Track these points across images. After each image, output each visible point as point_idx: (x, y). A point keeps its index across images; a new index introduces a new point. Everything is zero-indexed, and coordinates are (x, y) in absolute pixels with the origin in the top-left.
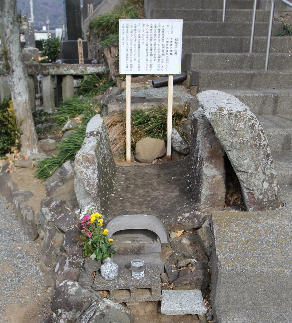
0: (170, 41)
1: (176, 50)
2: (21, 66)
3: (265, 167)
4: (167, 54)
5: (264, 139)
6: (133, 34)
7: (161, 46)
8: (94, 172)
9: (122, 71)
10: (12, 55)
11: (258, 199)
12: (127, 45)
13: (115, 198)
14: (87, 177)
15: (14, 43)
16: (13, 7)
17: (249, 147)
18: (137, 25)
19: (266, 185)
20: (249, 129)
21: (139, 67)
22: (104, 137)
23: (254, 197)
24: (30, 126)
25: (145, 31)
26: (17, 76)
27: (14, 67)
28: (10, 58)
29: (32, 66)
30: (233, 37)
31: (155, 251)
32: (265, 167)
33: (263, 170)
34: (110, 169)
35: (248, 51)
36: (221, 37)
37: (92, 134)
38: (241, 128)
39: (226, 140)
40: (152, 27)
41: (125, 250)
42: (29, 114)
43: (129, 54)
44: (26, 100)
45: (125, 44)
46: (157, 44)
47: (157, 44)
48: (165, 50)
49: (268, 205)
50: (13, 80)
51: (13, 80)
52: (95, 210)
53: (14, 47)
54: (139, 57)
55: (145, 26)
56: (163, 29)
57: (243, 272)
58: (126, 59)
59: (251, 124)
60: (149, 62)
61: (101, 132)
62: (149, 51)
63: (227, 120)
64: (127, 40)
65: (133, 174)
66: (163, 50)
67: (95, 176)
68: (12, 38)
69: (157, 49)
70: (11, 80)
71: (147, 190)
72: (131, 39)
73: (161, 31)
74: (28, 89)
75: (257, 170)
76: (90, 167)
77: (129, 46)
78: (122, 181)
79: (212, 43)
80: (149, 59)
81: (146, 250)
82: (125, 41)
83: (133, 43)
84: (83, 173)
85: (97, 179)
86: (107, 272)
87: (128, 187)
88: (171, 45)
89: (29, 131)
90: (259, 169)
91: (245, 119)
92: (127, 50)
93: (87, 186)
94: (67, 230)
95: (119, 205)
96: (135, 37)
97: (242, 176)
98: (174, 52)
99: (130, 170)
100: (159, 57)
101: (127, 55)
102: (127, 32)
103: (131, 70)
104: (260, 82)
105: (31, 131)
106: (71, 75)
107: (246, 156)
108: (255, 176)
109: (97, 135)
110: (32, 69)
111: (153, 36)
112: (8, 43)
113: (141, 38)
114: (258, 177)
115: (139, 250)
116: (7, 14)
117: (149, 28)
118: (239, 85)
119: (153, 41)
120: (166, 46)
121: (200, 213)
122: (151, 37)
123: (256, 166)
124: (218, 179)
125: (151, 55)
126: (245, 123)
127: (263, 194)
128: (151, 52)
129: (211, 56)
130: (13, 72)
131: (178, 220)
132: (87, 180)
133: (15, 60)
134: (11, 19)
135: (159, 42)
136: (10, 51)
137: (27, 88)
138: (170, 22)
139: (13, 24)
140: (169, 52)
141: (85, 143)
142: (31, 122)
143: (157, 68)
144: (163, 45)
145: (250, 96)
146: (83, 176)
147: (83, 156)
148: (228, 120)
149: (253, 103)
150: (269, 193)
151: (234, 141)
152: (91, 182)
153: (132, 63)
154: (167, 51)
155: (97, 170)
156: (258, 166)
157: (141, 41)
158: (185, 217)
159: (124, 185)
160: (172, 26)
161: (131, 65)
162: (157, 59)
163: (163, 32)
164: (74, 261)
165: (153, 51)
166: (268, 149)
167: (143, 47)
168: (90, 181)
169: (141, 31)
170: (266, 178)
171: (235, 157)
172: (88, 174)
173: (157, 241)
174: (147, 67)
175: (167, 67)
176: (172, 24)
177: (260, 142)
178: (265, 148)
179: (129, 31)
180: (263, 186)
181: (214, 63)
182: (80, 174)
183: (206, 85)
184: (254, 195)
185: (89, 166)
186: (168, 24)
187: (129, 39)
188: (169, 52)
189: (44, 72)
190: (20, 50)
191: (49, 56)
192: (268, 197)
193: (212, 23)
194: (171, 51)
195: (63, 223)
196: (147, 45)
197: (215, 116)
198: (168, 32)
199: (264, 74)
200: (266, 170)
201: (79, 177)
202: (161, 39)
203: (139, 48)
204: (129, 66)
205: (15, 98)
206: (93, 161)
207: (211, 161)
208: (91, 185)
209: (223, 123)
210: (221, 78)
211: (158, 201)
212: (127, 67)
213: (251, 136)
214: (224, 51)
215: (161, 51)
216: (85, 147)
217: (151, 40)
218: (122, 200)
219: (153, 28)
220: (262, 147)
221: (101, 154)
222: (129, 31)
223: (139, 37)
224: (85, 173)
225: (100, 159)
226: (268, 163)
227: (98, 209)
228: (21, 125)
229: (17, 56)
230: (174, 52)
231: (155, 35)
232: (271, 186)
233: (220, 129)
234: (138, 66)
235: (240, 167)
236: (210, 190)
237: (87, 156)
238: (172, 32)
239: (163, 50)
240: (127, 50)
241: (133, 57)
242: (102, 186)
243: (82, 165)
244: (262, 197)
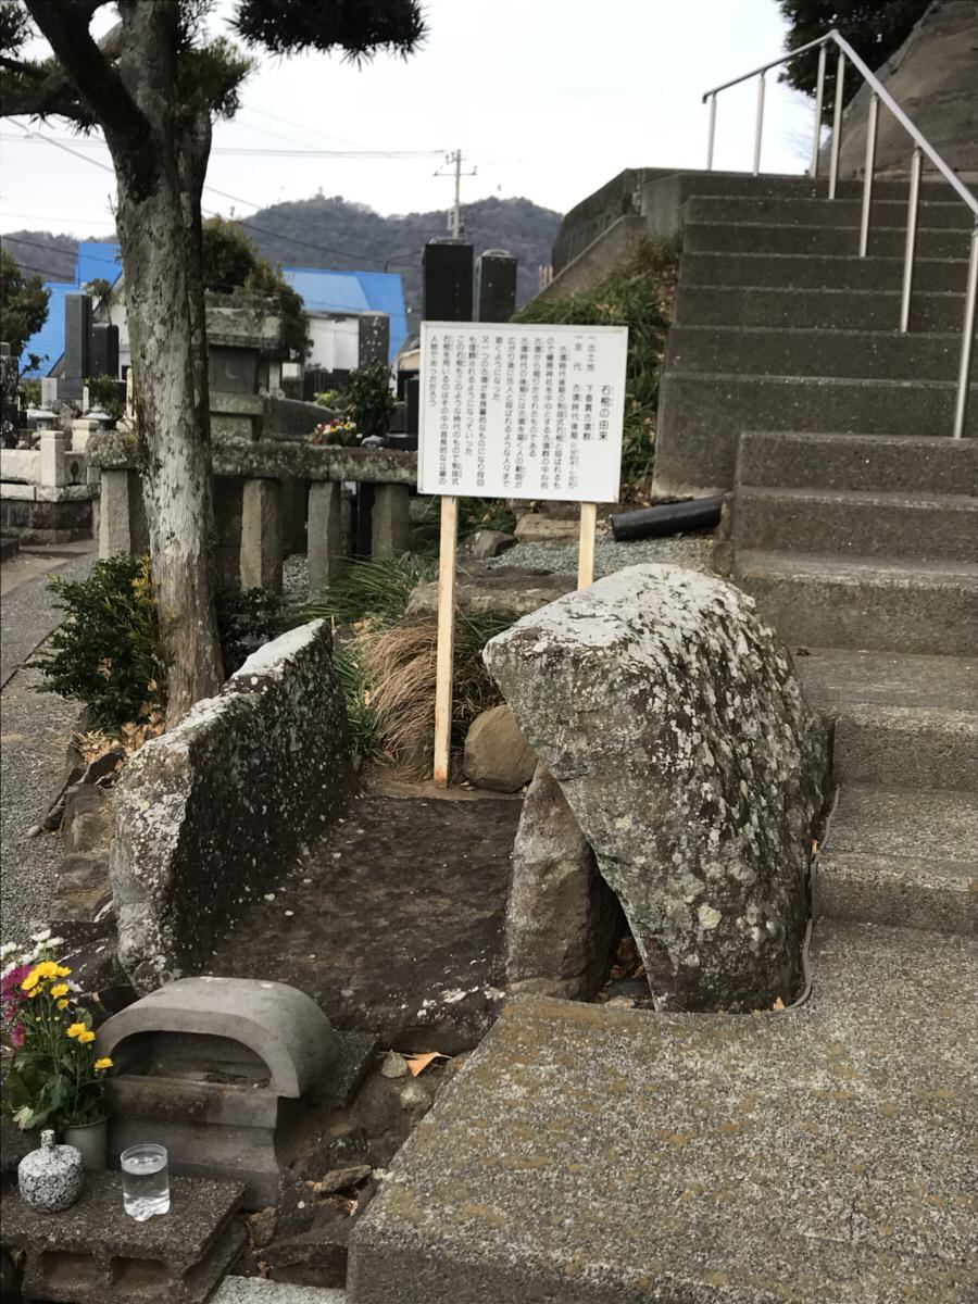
0: (583, 393)
1: (604, 424)
2: (185, 452)
3: (698, 851)
4: (574, 435)
5: (688, 750)
6: (465, 370)
7: (555, 410)
10: (157, 418)
11: (683, 968)
12: (445, 402)
14: (145, 829)
15: (167, 379)
16: (172, 273)
17: (630, 774)
18: (479, 342)
19: (709, 918)
20: (629, 709)
21: (481, 474)
23: (668, 958)
24: (199, 639)
25: (505, 361)
26: (170, 481)
27: (162, 455)
28: (153, 424)
29: (276, 453)
30: (906, 384)
31: (255, 1123)
32: (698, 851)
33: (690, 861)
35: (950, 433)
36: (866, 382)
38: (597, 703)
39: (546, 744)
40: (525, 349)
41: (156, 1106)
42: (197, 602)
43: (450, 431)
44: (190, 556)
45: (439, 400)
46: (542, 402)
47: (542, 402)
48: (568, 422)
49: (725, 993)
50: (157, 493)
51: (157, 493)
52: (153, 946)
53: (165, 394)
54: (482, 443)
55: (505, 346)
56: (564, 357)
57: (434, 1247)
58: (439, 446)
59: (637, 692)
62: (515, 425)
63: (543, 672)
64: (445, 386)
66: (560, 422)
67: (174, 829)
68: (161, 364)
69: (540, 420)
70: (150, 493)
72: (459, 386)
73: (557, 361)
74: (200, 522)
75: (670, 859)
76: (165, 798)
77: (452, 405)
79: (832, 399)
80: (514, 450)
81: (226, 1117)
82: (439, 391)
83: (465, 397)
84: (137, 816)
85: (176, 838)
88: (588, 407)
89: (193, 654)
90: (677, 857)
91: (611, 676)
93: (138, 862)
96: (471, 380)
97: (617, 876)
98: (595, 431)
100: (547, 445)
101: (444, 434)
102: (446, 362)
103: (455, 482)
104: (953, 541)
105: (199, 654)
107: (621, 803)
108: (663, 880)
110: (276, 460)
111: (530, 377)
112: (150, 380)
113: (491, 383)
114: (677, 886)
115: (200, 1112)
116: (150, 293)
117: (518, 352)
118: (875, 544)
119: (529, 395)
120: (570, 411)
121: (502, 995)
122: (524, 382)
123: (661, 842)
124: (562, 877)
125: (520, 438)
126: (611, 690)
127: (701, 952)
128: (521, 429)
129: (806, 444)
130: (158, 467)
131: (420, 1013)
133: (168, 433)
134: (161, 309)
135: (549, 398)
136: (152, 404)
137: (196, 521)
138: (586, 335)
139: (169, 324)
140: (581, 431)
142: (202, 627)
143: (540, 481)
144: (560, 405)
145: (878, 588)
146: (134, 826)
148: (548, 676)
149: (889, 611)
150: (726, 947)
151: (573, 748)
153: (459, 461)
154: (575, 426)
156: (670, 844)
157: (490, 392)
158: (446, 1004)
160: (592, 348)
161: (454, 465)
162: (539, 449)
163: (562, 366)
165: (527, 426)
166: (706, 786)
167: (496, 410)
168: (151, 844)
169: (491, 360)
170: (706, 891)
171: (582, 804)
172: (150, 821)
174: (506, 476)
175: (572, 478)
176: (591, 342)
177: (672, 758)
178: (693, 782)
179: (453, 358)
180: (696, 920)
181: (814, 468)
183: (759, 541)
184: (666, 948)
185: (162, 793)
186: (580, 341)
187: (452, 383)
188: (581, 431)
189: (313, 470)
190: (183, 401)
191: (361, 422)
192: (723, 962)
193: (856, 337)
194: (588, 426)
196: (509, 405)
197: (503, 658)
198: (577, 365)
199: (968, 512)
200: (703, 861)
202: (555, 387)
203: (483, 412)
204: (449, 470)
205: (157, 549)
206: (180, 776)
207: (547, 811)
209: (531, 683)
210: (813, 519)
211: (406, 933)
212: (443, 474)
213: (637, 734)
214: (876, 429)
215: (553, 426)
217: (522, 389)
218: (290, 917)
219: (531, 353)
220: (680, 779)
222: (453, 358)
223: (485, 379)
224: (141, 816)
226: (707, 837)
227: (164, 945)
228: (170, 633)
229: (175, 421)
230: (595, 431)
231: (537, 374)
232: (733, 923)
233: (521, 702)
235: (604, 843)
236: (534, 915)
238: (591, 367)
239: (560, 422)
240: (444, 419)
241: (462, 440)
244: (697, 960)
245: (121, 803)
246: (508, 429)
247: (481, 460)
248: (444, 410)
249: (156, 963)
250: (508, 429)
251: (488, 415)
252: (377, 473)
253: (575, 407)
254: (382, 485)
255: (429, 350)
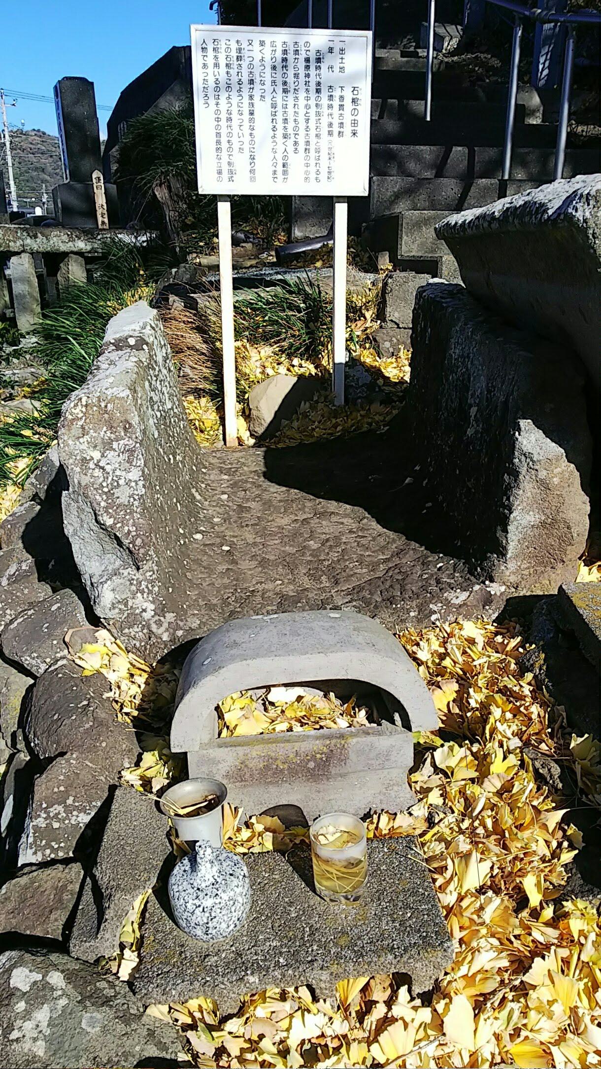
1: (355, 123)
8: (130, 462)
9: (207, 184)
13: (205, 545)
14: (106, 479)
18: (245, 45)
21: (252, 171)
22: (160, 359)
34: (184, 458)
37: (120, 344)
43: (224, 131)
48: (325, 121)
52: (139, 595)
60: (279, 156)
61: (151, 340)
62: (280, 125)
65: (251, 472)
71: (302, 517)
76: (115, 445)
78: (223, 493)
84: (92, 465)
85: (141, 483)
86: (198, 911)
87: (241, 509)
88: (341, 107)
92: (218, 120)
94: (43, 667)
95: (222, 568)
98: (348, 129)
99: (242, 460)
101: (218, 134)
103: (231, 179)
106: (80, 253)
109: (138, 347)
122: (285, 83)
125: (285, 136)
132: (106, 490)
140: (336, 129)
141: (98, 368)
146: (92, 476)
147: (86, 406)
152: (123, 495)
153: (233, 159)
154: (331, 125)
155: (139, 452)
159: (230, 504)
161: (229, 164)
162: (302, 147)
164: (56, 825)
165: (291, 125)
172: (108, 468)
173: (393, 722)
174: (275, 172)
176: (341, 45)
179: (222, 62)
182: (78, 470)
188: (336, 129)
189: (12, 244)
194: (341, 125)
195: (28, 644)
196: (274, 106)
201: (76, 481)
203: (252, 114)
204: (225, 168)
208: (120, 505)
216: (96, 379)
221: (152, 406)
225: (151, 422)
230: (348, 129)
234: (249, 168)
237: (103, 405)
240: (218, 120)
241: (234, 140)
242: (162, 507)
243: (87, 438)
245: (71, 454)
246: (274, 129)
247: (253, 158)
248: (218, 111)
249: (144, 610)
250: (274, 129)
251: (256, 115)
252: (61, 244)
253: (330, 107)
254: (65, 255)
255: (200, 53)
